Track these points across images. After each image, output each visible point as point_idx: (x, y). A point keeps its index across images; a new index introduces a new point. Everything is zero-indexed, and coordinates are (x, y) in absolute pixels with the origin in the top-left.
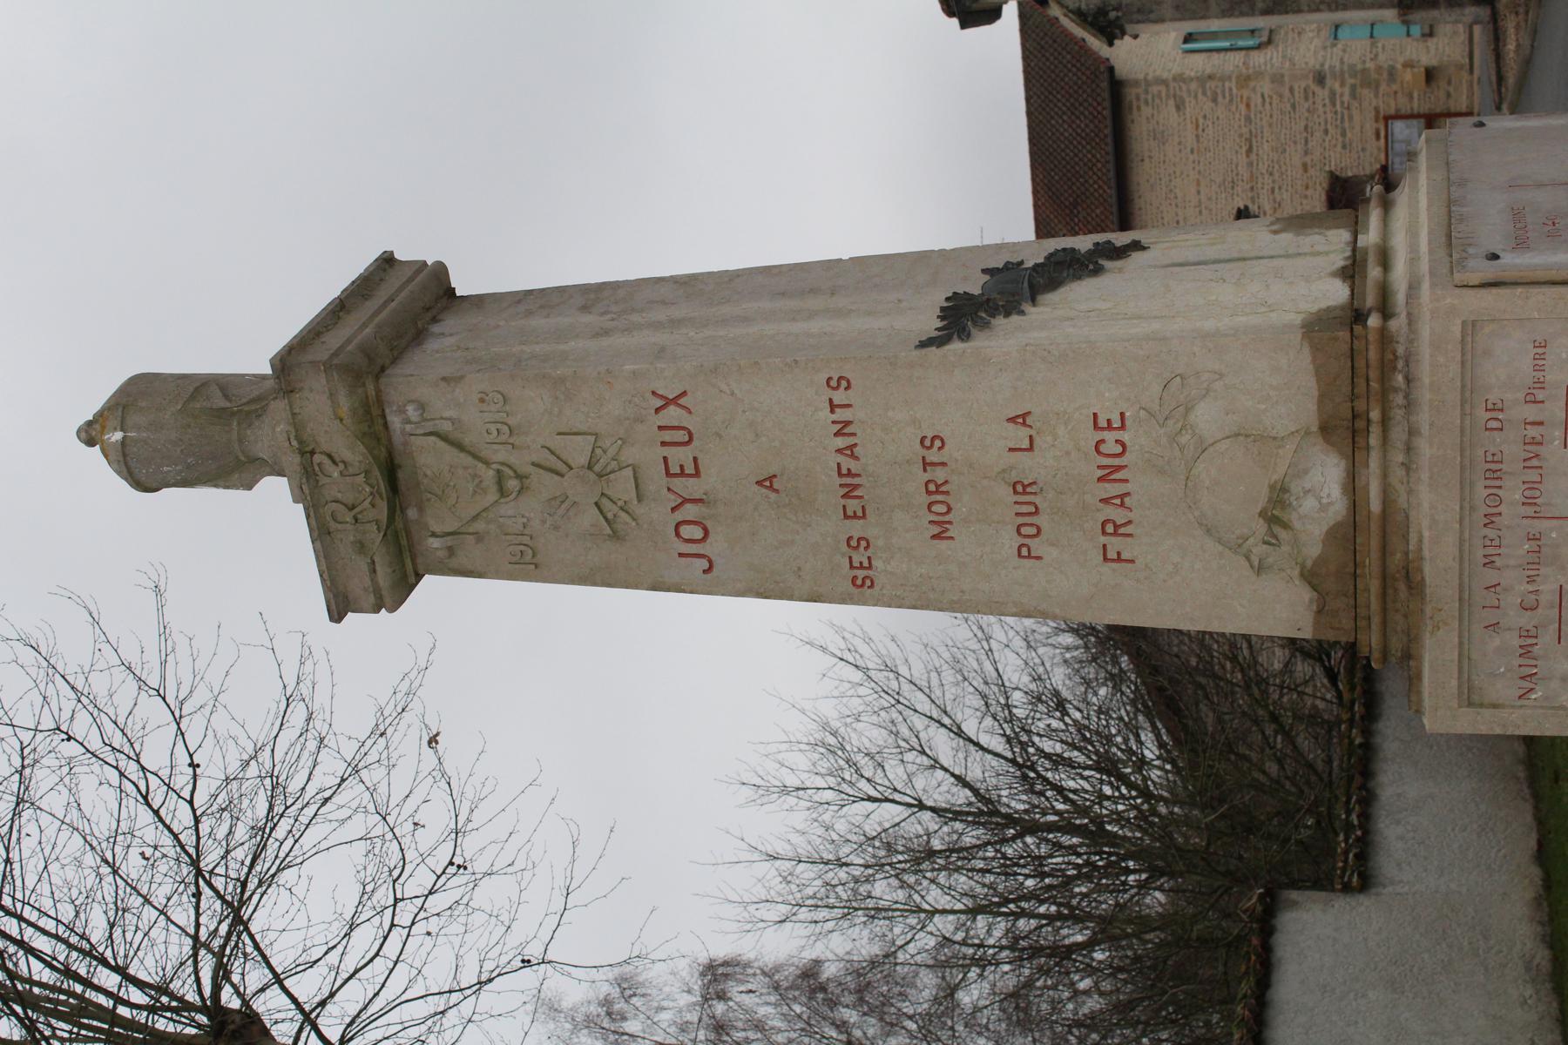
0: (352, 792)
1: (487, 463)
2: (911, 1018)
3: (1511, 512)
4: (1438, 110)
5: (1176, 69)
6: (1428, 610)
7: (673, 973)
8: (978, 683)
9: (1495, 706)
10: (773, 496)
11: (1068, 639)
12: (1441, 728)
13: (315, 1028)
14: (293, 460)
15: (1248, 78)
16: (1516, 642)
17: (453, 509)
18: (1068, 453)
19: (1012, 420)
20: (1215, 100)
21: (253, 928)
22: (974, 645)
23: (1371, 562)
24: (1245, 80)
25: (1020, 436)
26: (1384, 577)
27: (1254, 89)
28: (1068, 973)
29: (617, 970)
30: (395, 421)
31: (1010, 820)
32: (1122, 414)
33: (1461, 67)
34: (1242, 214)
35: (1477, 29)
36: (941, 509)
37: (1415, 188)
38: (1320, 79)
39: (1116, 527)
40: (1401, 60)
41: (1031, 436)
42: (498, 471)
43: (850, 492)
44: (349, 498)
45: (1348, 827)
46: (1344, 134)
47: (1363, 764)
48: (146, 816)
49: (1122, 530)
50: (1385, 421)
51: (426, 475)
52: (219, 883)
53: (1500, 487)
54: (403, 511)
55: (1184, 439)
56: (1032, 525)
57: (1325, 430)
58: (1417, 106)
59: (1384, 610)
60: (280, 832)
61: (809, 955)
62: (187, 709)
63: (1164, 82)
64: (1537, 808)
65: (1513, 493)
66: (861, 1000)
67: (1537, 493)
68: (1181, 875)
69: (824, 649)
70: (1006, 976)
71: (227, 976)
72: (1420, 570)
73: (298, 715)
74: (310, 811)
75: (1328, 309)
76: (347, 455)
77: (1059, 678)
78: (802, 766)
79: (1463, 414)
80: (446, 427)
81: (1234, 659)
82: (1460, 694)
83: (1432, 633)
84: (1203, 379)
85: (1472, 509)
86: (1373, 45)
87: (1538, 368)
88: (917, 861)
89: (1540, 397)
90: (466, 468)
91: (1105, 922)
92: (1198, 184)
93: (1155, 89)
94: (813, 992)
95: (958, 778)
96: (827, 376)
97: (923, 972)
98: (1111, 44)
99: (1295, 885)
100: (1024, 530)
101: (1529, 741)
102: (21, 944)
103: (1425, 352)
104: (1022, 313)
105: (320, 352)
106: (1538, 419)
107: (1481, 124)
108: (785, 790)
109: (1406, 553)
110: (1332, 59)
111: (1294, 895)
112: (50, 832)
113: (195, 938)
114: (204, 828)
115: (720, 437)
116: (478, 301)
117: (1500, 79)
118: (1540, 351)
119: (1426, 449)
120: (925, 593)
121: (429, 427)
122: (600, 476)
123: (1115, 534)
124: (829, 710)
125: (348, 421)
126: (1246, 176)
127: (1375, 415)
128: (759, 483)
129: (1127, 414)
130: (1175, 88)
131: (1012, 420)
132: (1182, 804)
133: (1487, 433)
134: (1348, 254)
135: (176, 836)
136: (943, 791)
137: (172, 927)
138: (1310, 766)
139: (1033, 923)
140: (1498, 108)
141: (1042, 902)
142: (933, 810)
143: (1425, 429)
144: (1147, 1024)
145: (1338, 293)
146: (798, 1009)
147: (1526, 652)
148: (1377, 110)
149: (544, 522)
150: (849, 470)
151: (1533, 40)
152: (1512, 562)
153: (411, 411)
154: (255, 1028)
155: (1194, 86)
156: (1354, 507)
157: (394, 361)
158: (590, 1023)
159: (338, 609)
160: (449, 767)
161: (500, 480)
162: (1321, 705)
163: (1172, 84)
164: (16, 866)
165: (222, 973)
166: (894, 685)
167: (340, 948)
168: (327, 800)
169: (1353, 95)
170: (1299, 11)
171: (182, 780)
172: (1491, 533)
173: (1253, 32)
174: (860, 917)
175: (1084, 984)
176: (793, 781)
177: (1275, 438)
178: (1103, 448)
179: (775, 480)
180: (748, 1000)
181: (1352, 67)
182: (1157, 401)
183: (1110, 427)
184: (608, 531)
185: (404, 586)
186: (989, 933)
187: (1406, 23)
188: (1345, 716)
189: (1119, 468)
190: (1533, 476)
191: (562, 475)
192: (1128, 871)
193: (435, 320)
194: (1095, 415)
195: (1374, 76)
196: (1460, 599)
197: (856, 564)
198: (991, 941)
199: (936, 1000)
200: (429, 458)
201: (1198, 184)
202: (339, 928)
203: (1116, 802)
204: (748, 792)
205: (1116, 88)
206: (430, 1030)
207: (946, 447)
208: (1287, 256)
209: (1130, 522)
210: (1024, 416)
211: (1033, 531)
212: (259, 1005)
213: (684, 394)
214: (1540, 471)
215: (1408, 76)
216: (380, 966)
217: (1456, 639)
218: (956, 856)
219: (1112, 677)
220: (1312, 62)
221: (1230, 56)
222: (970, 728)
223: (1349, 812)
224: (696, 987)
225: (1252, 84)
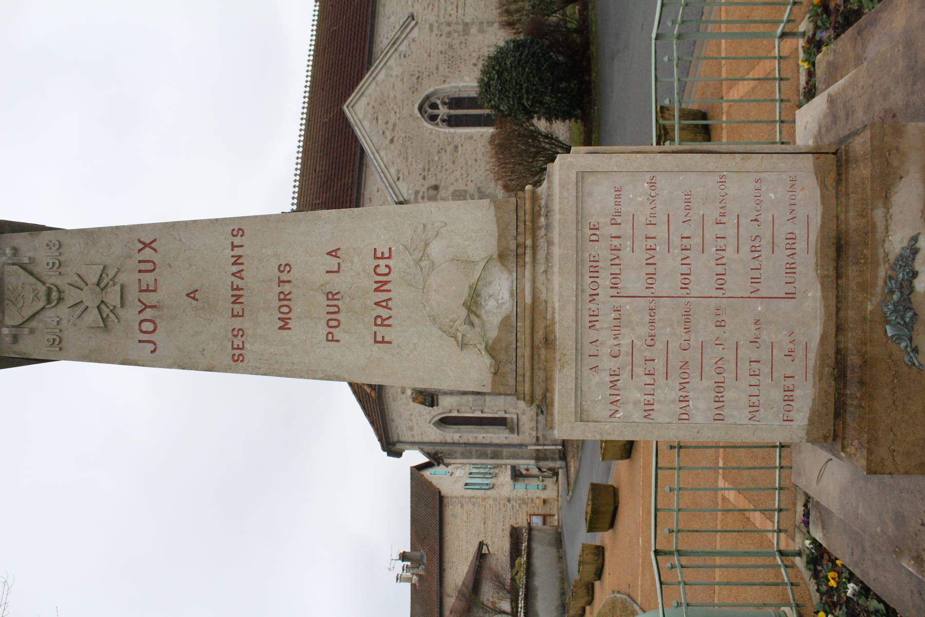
3: (604, 293)
4: (547, 513)
5: (461, 494)
6: (558, 356)
10: (194, 302)
15: (485, 499)
16: (608, 379)
17: (20, 311)
18: (359, 274)
19: (329, 253)
20: (474, 505)
24: (484, 499)
25: (333, 263)
27: (487, 503)
32: (390, 249)
33: (554, 499)
36: (285, 310)
38: (509, 501)
40: (535, 496)
41: (339, 263)
43: (236, 299)
49: (386, 323)
50: (534, 248)
51: (9, 289)
53: (598, 277)
55: (423, 264)
56: (335, 320)
58: (540, 512)
65: (605, 280)
67: (618, 281)
79: (577, 230)
82: (576, 412)
83: (560, 370)
84: (436, 225)
85: (583, 291)
86: (526, 491)
87: (618, 204)
89: (619, 221)
90: (31, 285)
92: (467, 533)
93: (454, 500)
96: (233, 228)
103: (556, 206)
106: (618, 234)
110: (513, 494)
115: (170, 266)
117: (568, 484)
118: (618, 193)
119: (556, 251)
120: (272, 365)
121: (16, 260)
126: (483, 532)
127: (529, 242)
129: (393, 249)
131: (329, 253)
133: (591, 243)
147: (613, 385)
149: (69, 321)
150: (237, 285)
151: (580, 463)
152: (605, 326)
155: (467, 500)
161: (49, 291)
163: (460, 499)
170: (503, 459)
173: (487, 484)
177: (473, 262)
178: (379, 271)
179: (197, 293)
181: (519, 497)
182: (410, 241)
183: (383, 258)
184: (102, 325)
189: (386, 283)
190: (616, 270)
194: (375, 249)
195: (526, 500)
196: (576, 348)
197: (236, 346)
201: (467, 533)
207: (292, 271)
209: (390, 317)
210: (336, 250)
213: (155, 240)
214: (619, 267)
215: (538, 501)
217: (574, 375)
220: (506, 495)
221: (480, 491)
225: (487, 500)
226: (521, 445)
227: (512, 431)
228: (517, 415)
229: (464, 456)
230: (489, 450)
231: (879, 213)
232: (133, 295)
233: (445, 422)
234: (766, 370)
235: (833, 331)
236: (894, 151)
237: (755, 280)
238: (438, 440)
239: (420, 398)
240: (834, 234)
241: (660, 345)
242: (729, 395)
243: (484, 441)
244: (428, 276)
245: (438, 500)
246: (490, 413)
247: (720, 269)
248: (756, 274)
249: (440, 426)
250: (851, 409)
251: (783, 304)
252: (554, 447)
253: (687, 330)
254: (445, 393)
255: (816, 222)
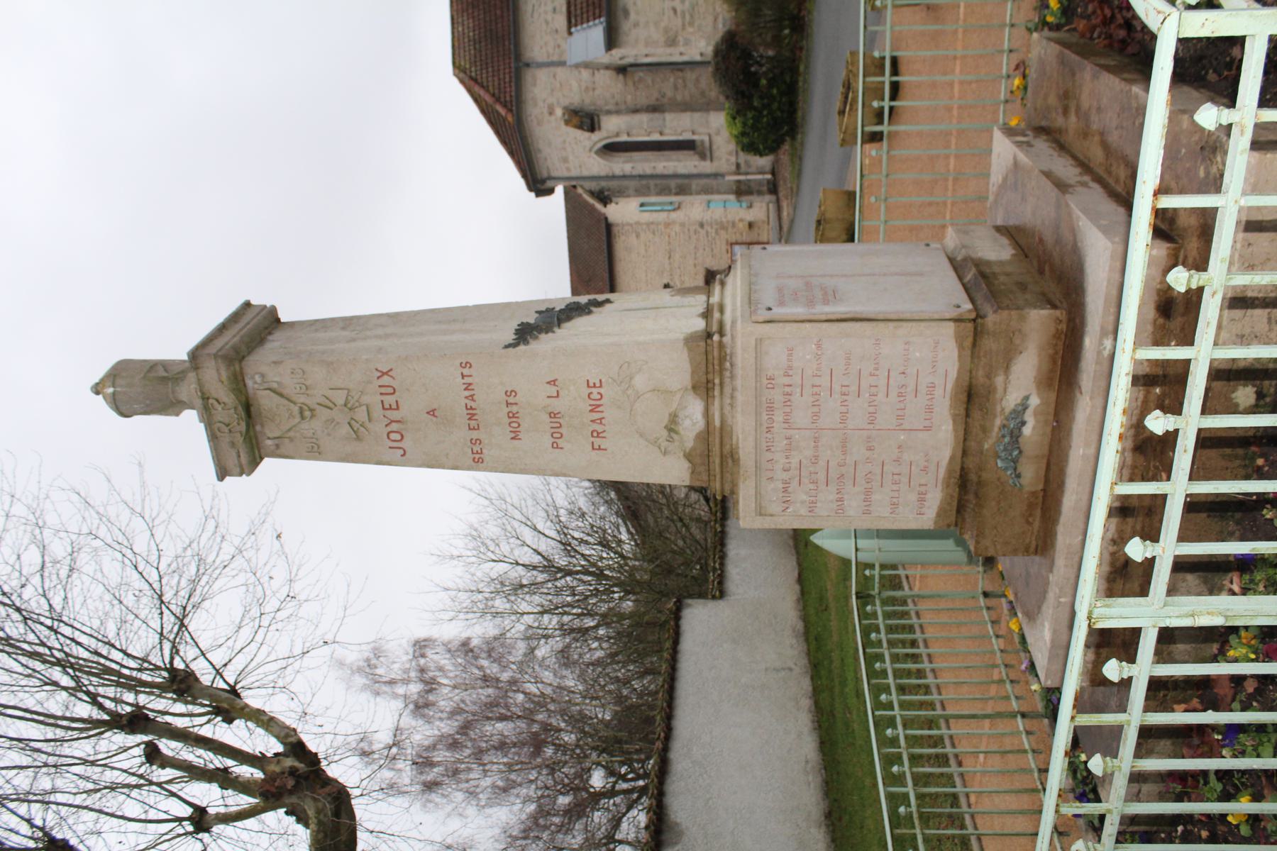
0: (239, 561)
1: (295, 403)
2: (513, 663)
3: (778, 426)
6: (741, 472)
7: (400, 646)
8: (544, 505)
9: (772, 515)
10: (434, 419)
11: (587, 484)
12: (748, 527)
13: (222, 677)
14: (199, 402)
18: (575, 399)
19: (548, 383)
21: (190, 629)
22: (542, 487)
23: (716, 449)
24: (667, 225)
25: (552, 390)
26: (722, 456)
28: (586, 641)
29: (372, 645)
30: (249, 383)
31: (560, 570)
33: (763, 222)
34: (666, 286)
35: (771, 205)
37: (735, 276)
38: (702, 225)
39: (598, 433)
42: (301, 408)
43: (471, 417)
44: (227, 421)
45: (714, 569)
46: (712, 250)
47: (721, 540)
48: (136, 575)
50: (721, 384)
52: (173, 607)
54: (253, 426)
55: (630, 392)
57: (694, 388)
59: (722, 472)
60: (203, 582)
61: (465, 635)
62: (156, 522)
63: (631, 225)
64: (798, 559)
65: (778, 417)
66: (490, 656)
68: (638, 593)
69: (471, 490)
70: (557, 643)
71: (177, 652)
72: (737, 453)
73: (211, 524)
74: (217, 572)
75: (696, 332)
76: (225, 399)
77: (583, 503)
78: (460, 546)
79: (756, 382)
80: (275, 386)
81: (662, 493)
85: (761, 425)
87: (789, 360)
88: (515, 590)
91: (604, 616)
94: (466, 653)
95: (535, 550)
97: (519, 642)
98: (605, 206)
99: (691, 596)
100: (555, 435)
101: (795, 530)
102: (73, 640)
103: (739, 351)
104: (553, 332)
105: (213, 349)
107: (765, 248)
108: (452, 557)
109: (732, 445)
110: (707, 216)
111: (689, 601)
112: (87, 584)
113: (161, 634)
114: (164, 581)
116: (291, 325)
119: (740, 397)
121: (266, 386)
122: (350, 409)
123: (598, 437)
124: (474, 519)
125: (226, 383)
127: (717, 381)
128: (428, 413)
130: (636, 228)
131: (548, 383)
132: (638, 560)
134: (705, 306)
135: (151, 585)
136: (529, 557)
137: (150, 630)
138: (697, 542)
139: (570, 617)
140: (780, 241)
141: (574, 607)
142: (523, 565)
143: (739, 387)
144: (624, 662)
145: (700, 324)
146: (460, 660)
147: (785, 490)
148: (727, 241)
151: (795, 211)
153: (258, 378)
154: (192, 678)
155: (644, 227)
156: (708, 423)
157: (249, 353)
158: (360, 670)
159: (222, 474)
160: (287, 550)
161: (301, 412)
162: (702, 513)
164: (70, 601)
165: (175, 651)
166: (504, 506)
167: (233, 638)
168: (225, 566)
169: (717, 233)
170: (691, 194)
171: (153, 559)
172: (769, 436)
174: (489, 617)
175: (595, 645)
176: (456, 553)
178: (592, 396)
180: (436, 657)
181: (716, 220)
183: (594, 386)
185: (254, 463)
186: (550, 623)
187: (739, 201)
188: (713, 518)
189: (599, 406)
190: (788, 409)
191: (331, 409)
192: (614, 592)
193: (270, 333)
198: (551, 627)
199: (525, 655)
200: (266, 401)
202: (233, 628)
203: (608, 559)
204: (434, 558)
205: (609, 227)
206: (279, 677)
208: (677, 307)
210: (554, 381)
211: (559, 435)
212: (193, 666)
213: (391, 370)
215: (741, 225)
216: (254, 646)
218: (534, 587)
219: (606, 502)
221: (661, 213)
222: (540, 527)
223: (715, 562)
224: (411, 651)
226: (716, 175)
227: (703, 156)
228: (710, 136)
229: (639, 192)
230: (673, 183)
231: (999, 380)
232: (377, 412)
233: (612, 148)
234: (905, 480)
235: (959, 454)
236: (1017, 333)
237: (900, 417)
238: (603, 173)
239: (575, 120)
240: (966, 384)
241: (822, 463)
242: (876, 497)
243: (666, 172)
244: (635, 401)
245: (604, 230)
246: (672, 135)
247: (872, 409)
248: (900, 413)
249: (605, 154)
250: (969, 510)
251: (921, 435)
252: (760, 177)
253: (844, 453)
254: (609, 112)
255: (953, 374)
